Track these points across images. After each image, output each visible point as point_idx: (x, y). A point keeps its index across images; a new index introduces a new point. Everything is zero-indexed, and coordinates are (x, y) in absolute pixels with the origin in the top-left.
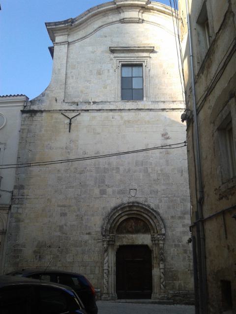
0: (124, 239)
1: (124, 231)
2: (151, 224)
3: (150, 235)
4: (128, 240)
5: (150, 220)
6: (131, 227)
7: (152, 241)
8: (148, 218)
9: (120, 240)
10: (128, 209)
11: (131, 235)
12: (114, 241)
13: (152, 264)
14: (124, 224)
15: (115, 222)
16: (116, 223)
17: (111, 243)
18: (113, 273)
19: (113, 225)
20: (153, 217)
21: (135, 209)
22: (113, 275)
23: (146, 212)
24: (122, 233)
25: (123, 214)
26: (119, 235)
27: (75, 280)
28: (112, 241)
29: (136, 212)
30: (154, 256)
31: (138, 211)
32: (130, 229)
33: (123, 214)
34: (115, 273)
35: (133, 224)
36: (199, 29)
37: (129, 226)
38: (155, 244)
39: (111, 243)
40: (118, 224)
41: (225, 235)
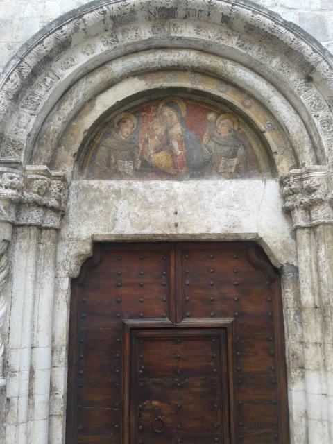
0: (122, 206)
1: (128, 166)
2: (280, 128)
3: (272, 186)
4: (148, 207)
5: (278, 103)
6: (165, 144)
7: (288, 212)
8: (262, 87)
9: (98, 209)
10: (145, 33)
11: (163, 184)
12: (61, 212)
13: (292, 344)
14: (126, 130)
15: (68, 108)
16: (78, 114)
17: (34, 216)
18: (40, 410)
19: (57, 124)
20: (293, 79)
21: (187, 32)
22: (40, 427)
23: (254, 53)
24: (111, 172)
25: (118, 67)
26: (94, 183)
27: (228, 176)
28: (37, 204)
29: (192, 57)
30: (308, 298)
31: (204, 49)
32: (160, 158)
33: (118, 67)
34: (60, 407)
35: (177, 129)
36: (287, 216)
37: (153, 142)
38: (312, 228)
39: (34, 216)
40: (89, 120)
41: (80, 83)
